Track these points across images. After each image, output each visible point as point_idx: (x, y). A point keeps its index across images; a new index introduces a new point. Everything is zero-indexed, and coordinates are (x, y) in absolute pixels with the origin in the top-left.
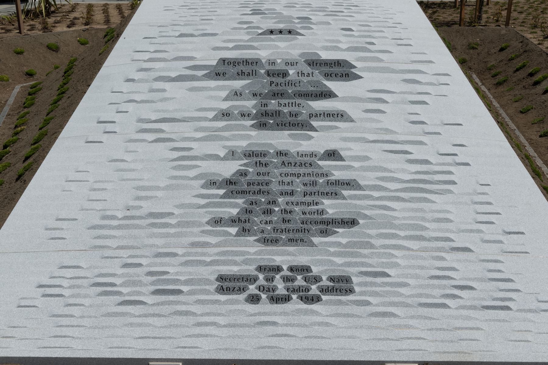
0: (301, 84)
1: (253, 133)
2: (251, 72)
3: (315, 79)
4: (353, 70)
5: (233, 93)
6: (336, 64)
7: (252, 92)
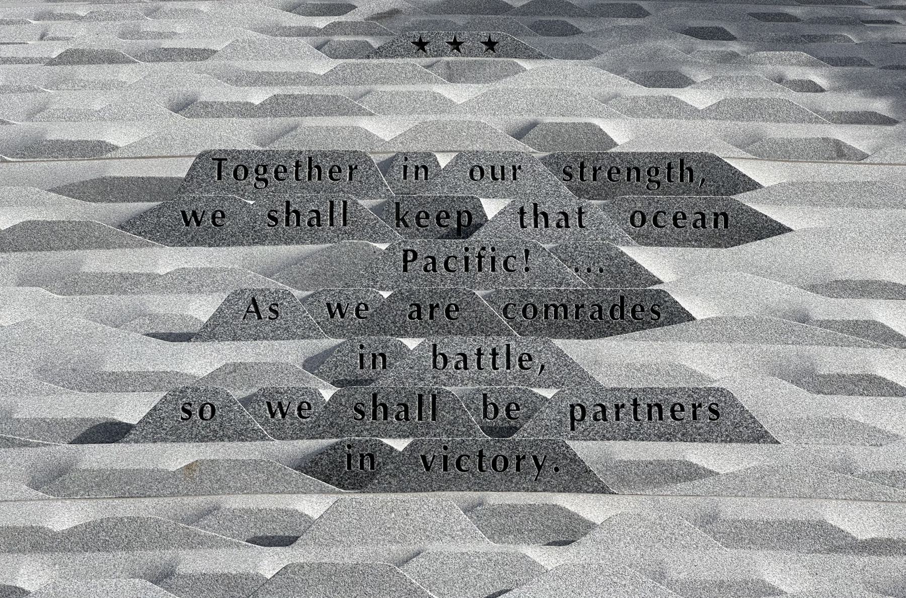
0: (536, 261)
1: (313, 504)
2: (324, 209)
3: (590, 235)
4: (744, 199)
5: (242, 305)
6: (676, 171)
7: (324, 299)
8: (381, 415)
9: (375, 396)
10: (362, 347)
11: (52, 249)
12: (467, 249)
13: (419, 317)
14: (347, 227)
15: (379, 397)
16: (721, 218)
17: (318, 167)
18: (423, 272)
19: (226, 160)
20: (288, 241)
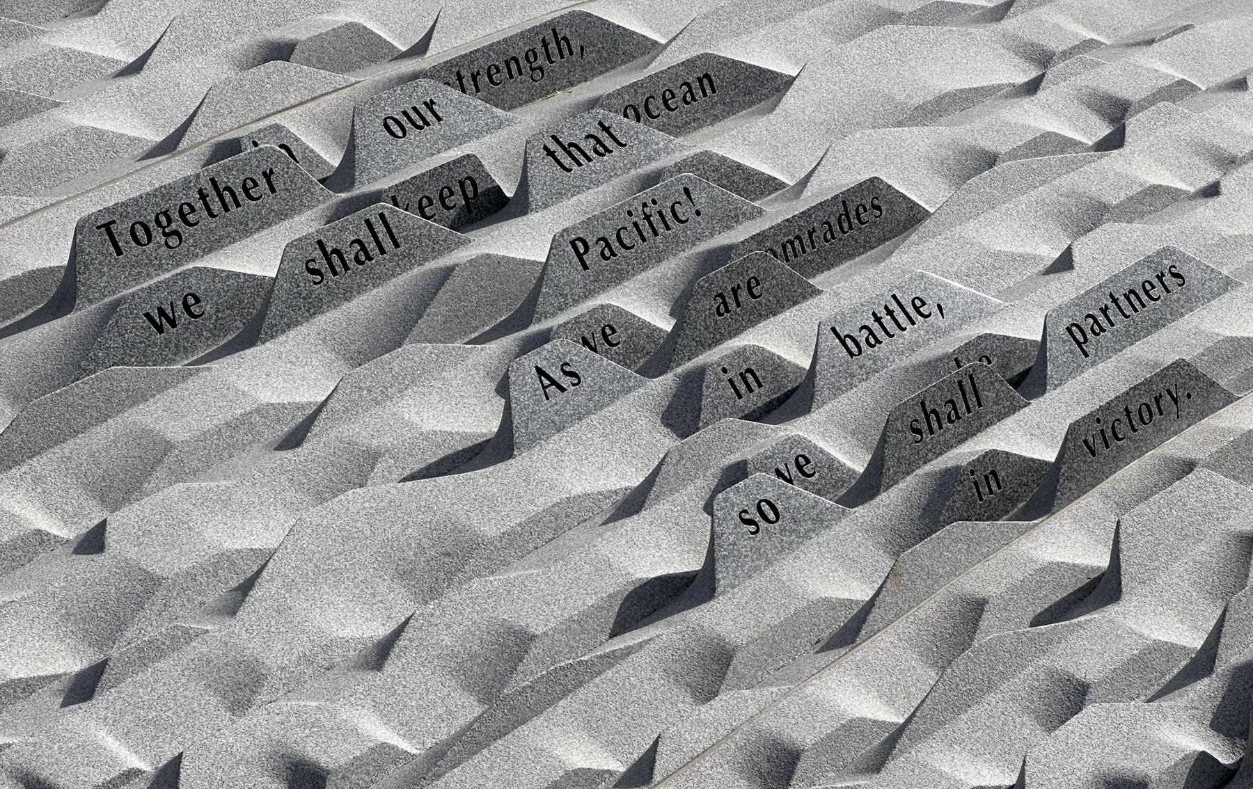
2: (364, 234)
8: (935, 426)
9: (923, 404)
10: (725, 370)
11: (77, 432)
12: (630, 213)
13: (727, 311)
14: (402, 248)
15: (927, 403)
16: (705, 81)
17: (227, 188)
18: (604, 262)
19: (114, 222)
20: (348, 295)
